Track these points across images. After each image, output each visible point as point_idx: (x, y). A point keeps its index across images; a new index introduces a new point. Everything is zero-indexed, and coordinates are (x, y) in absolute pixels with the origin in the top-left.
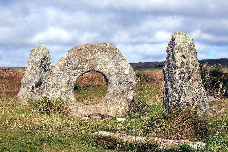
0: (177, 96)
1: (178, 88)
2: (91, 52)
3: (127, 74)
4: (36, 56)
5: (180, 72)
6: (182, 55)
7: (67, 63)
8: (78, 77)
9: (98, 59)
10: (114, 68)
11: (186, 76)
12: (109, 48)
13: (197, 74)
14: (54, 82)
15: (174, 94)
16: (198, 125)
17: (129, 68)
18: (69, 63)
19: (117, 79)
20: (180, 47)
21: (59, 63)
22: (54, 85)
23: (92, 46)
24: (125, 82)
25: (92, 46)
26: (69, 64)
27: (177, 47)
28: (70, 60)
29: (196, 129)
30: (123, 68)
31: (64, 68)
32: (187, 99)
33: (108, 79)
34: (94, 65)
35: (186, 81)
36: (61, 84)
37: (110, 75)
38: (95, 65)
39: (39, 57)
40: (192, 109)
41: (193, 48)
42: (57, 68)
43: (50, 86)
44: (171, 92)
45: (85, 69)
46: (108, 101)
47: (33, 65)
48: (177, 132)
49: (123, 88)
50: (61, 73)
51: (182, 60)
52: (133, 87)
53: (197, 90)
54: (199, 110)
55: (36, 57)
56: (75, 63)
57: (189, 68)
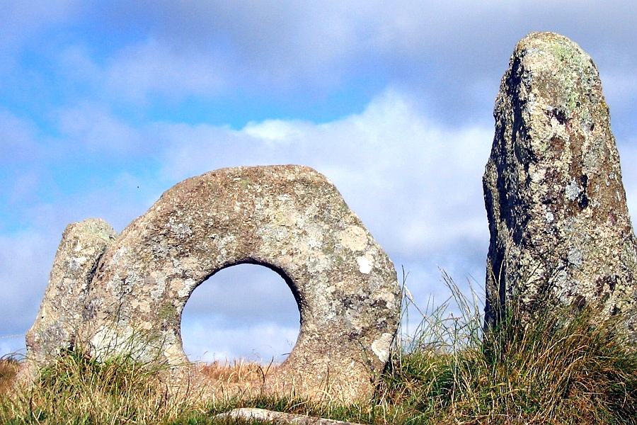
0: (538, 271)
1: (538, 237)
2: (241, 195)
3: (368, 272)
4: (76, 250)
5: (546, 175)
6: (554, 111)
7: (155, 233)
8: (194, 282)
9: (266, 220)
10: (320, 252)
11: (572, 192)
12: (303, 181)
13: (614, 191)
14: (111, 300)
15: (524, 262)
16: (624, 380)
17: (374, 253)
18: (164, 231)
19: (332, 289)
20: (547, 83)
21: (130, 233)
22: (111, 310)
23: (242, 177)
24: (360, 298)
25: (242, 177)
26: (165, 235)
27: (531, 81)
28: (167, 221)
29: (618, 394)
30: (354, 250)
31: (145, 250)
32: (577, 282)
33: (299, 290)
34: (251, 241)
35: (571, 214)
36: (134, 307)
37: (308, 276)
38: (254, 241)
39: (85, 252)
40: (599, 320)
41: (594, 92)
42: (122, 251)
43: (96, 315)
44: (514, 257)
45: (219, 253)
46: (303, 367)
47: (66, 280)
48: (539, 408)
49: (355, 322)
50: (137, 266)
51: (554, 131)
52: (388, 318)
53: (615, 252)
54: (622, 329)
55: (73, 254)
56: (183, 232)
57: (582, 162)
